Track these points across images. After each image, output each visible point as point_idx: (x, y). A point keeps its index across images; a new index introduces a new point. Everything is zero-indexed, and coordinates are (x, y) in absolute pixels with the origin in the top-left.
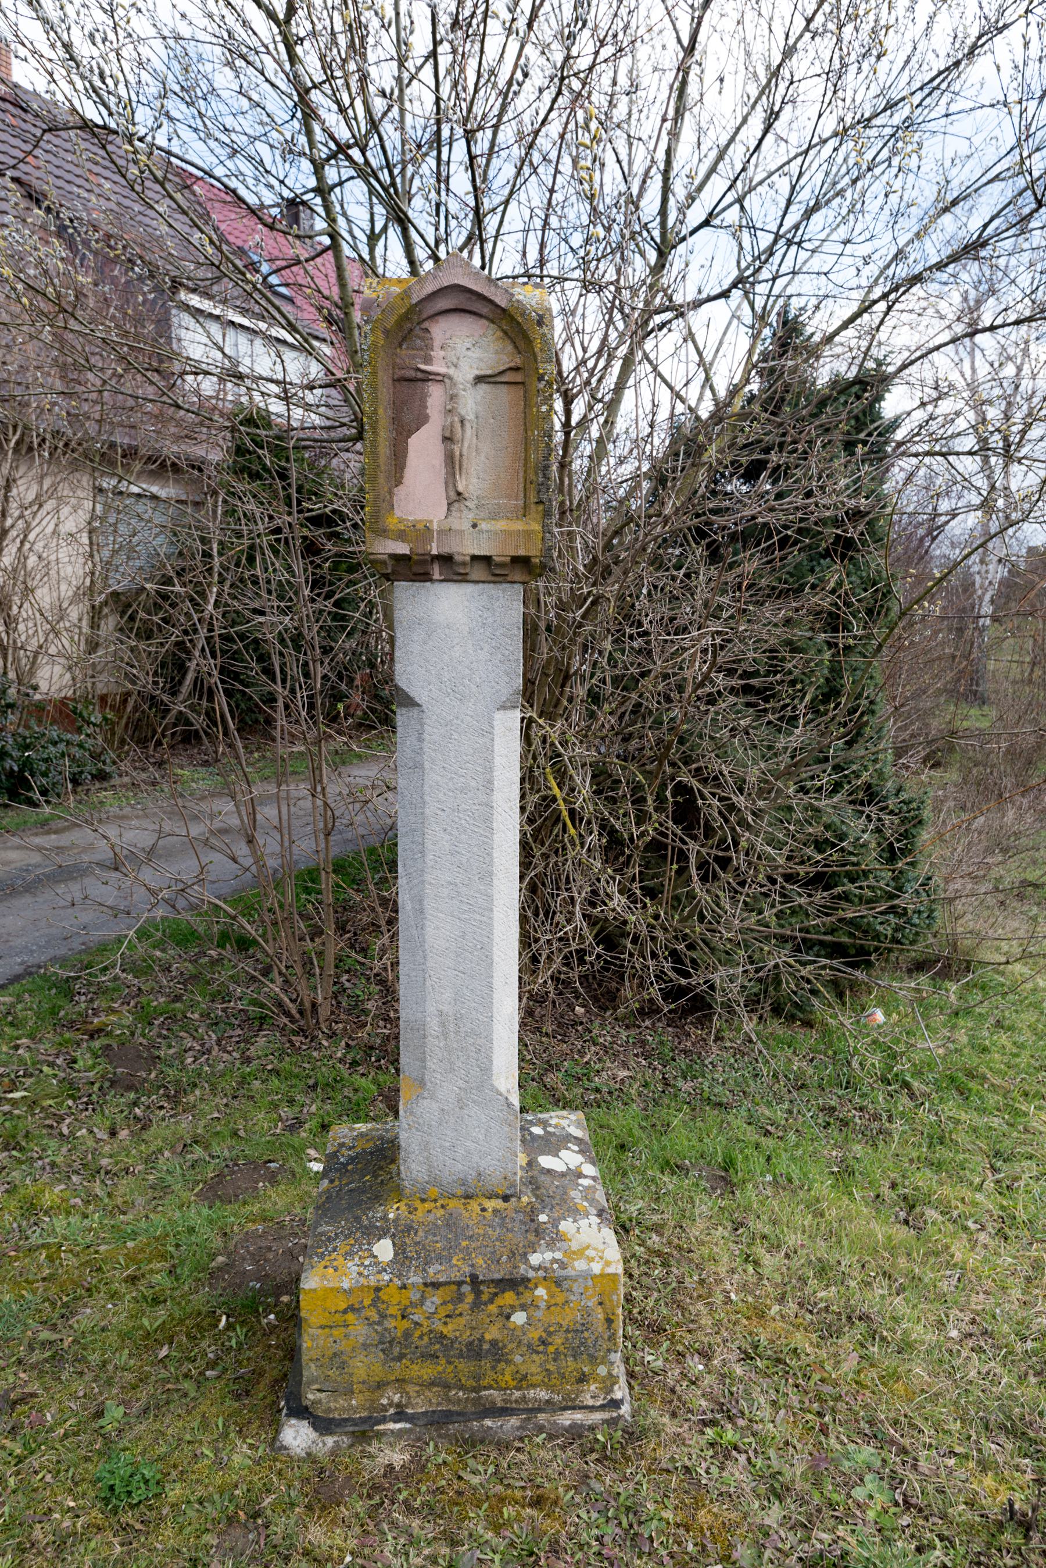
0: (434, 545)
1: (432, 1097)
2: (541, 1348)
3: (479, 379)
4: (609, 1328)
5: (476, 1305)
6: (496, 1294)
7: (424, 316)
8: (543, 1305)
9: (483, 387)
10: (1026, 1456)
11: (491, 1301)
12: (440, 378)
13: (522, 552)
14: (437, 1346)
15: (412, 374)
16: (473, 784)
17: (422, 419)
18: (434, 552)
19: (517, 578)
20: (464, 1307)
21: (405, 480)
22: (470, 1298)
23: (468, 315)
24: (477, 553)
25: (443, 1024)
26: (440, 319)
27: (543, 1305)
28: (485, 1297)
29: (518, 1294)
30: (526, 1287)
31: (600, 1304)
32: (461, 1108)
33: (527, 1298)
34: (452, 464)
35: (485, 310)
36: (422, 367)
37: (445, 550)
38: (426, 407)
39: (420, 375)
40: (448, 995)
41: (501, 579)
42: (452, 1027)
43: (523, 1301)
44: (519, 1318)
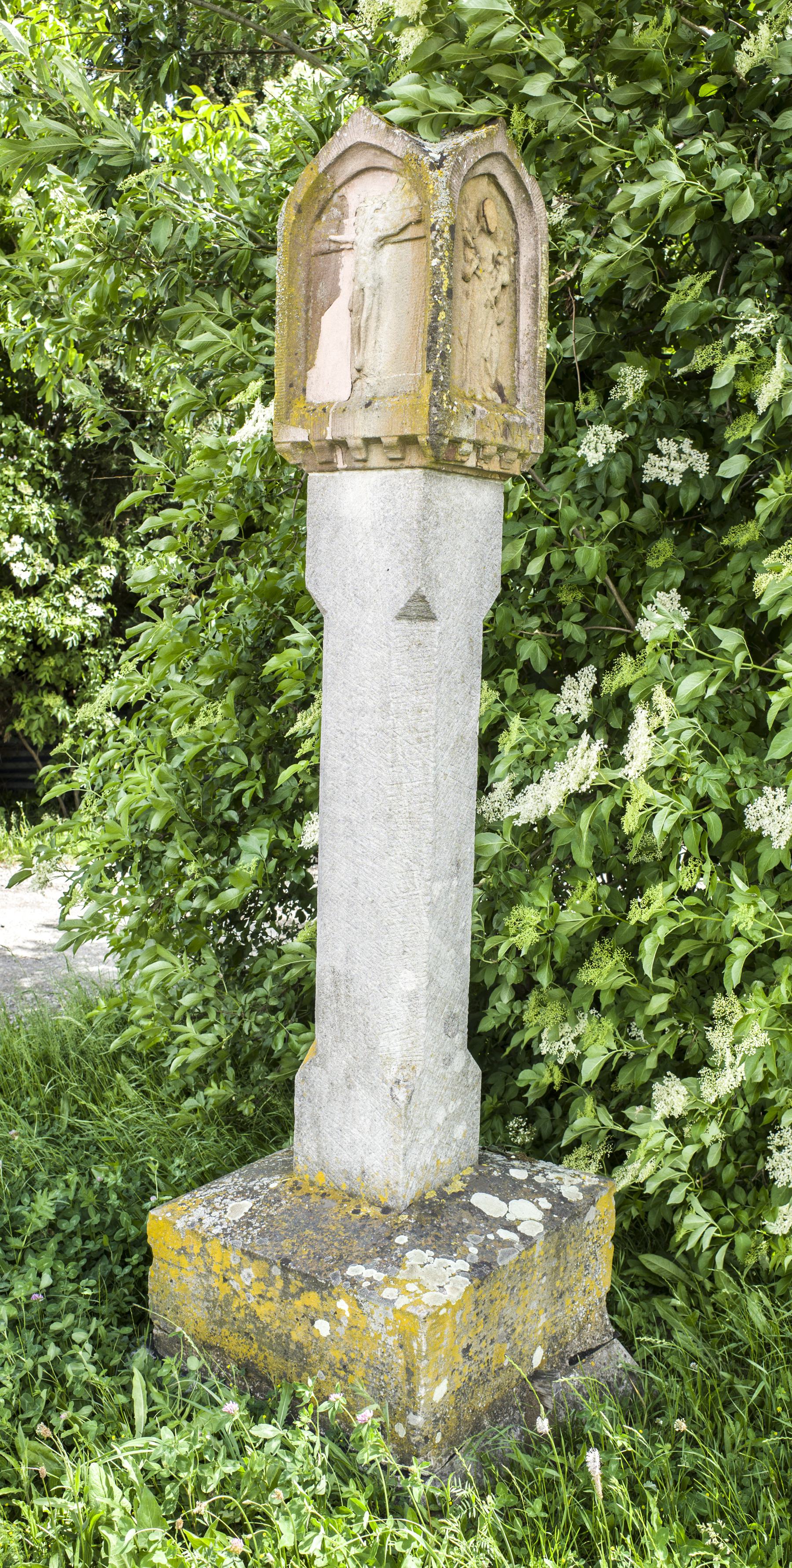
0: (329, 429)
1: (323, 1066)
2: (342, 1373)
3: (384, 240)
4: (409, 1381)
5: (285, 1294)
6: (302, 1290)
7: (338, 182)
8: (345, 1323)
9: (389, 249)
10: (61, 1213)
11: (297, 1295)
12: (349, 246)
13: (407, 431)
14: (251, 1326)
15: (325, 246)
16: (370, 704)
17: (335, 293)
18: (329, 437)
19: (414, 462)
20: (275, 1292)
21: (317, 362)
22: (280, 1284)
23: (376, 173)
24: (370, 435)
25: (335, 984)
26: (356, 182)
27: (345, 1323)
28: (293, 1289)
29: (323, 1299)
30: (330, 1294)
31: (401, 1346)
32: (349, 1087)
33: (328, 1306)
34: (358, 337)
35: (389, 163)
36: (332, 237)
37: (338, 435)
38: (338, 280)
39: (333, 246)
40: (341, 950)
41: (397, 464)
42: (343, 990)
43: (326, 1309)
44: (323, 1327)
